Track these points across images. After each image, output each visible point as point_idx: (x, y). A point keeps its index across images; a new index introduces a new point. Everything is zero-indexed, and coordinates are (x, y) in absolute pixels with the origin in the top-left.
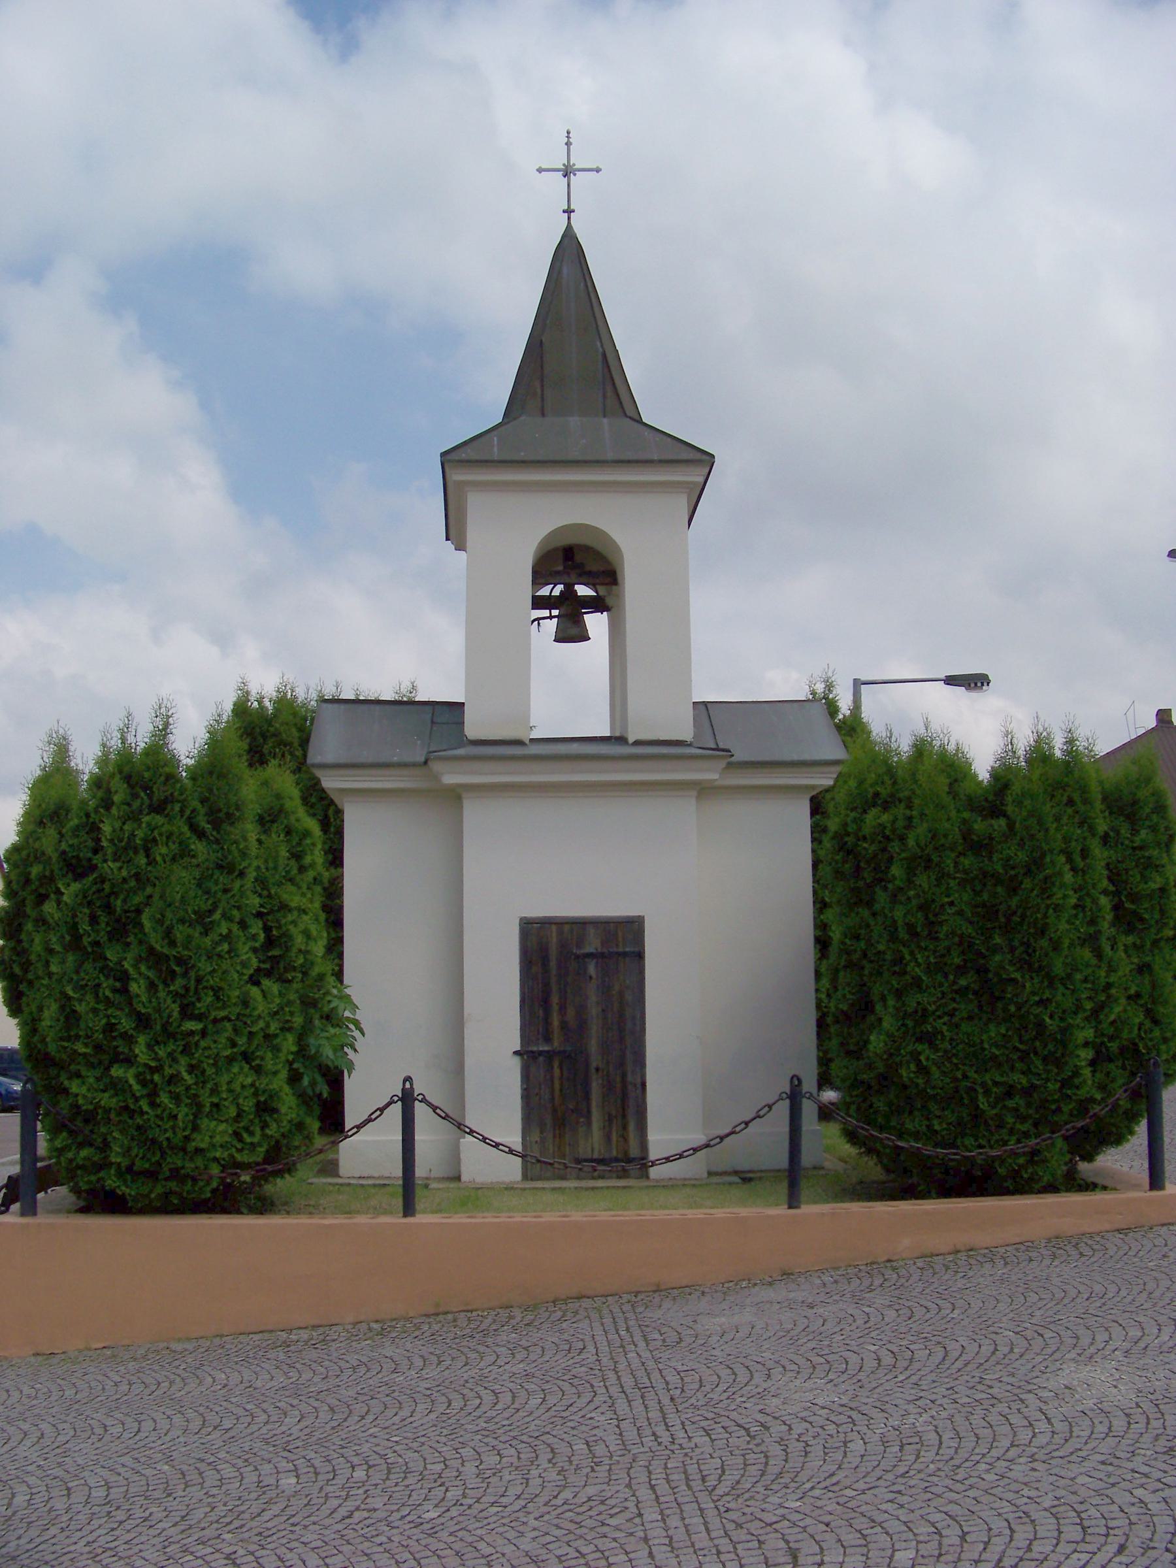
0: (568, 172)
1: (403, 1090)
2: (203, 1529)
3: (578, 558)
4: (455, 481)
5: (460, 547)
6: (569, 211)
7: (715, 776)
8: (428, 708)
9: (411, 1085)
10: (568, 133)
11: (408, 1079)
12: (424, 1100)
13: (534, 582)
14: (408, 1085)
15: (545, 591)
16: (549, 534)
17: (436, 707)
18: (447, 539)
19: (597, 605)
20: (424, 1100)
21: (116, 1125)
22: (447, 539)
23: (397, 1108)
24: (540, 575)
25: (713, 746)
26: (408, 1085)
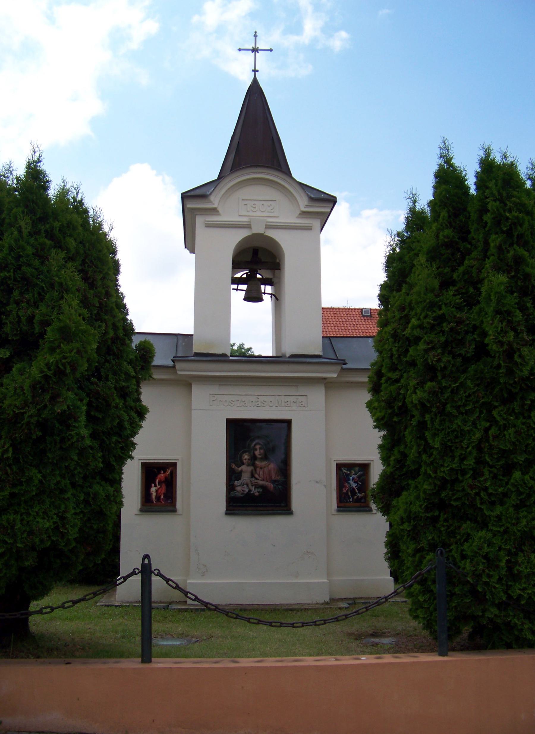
0: (255, 50)
1: (143, 565)
2: (90, 628)
3: (260, 255)
4: (188, 208)
5: (192, 251)
6: (255, 71)
7: (335, 375)
8: (174, 337)
9: (149, 561)
10: (256, 32)
11: (147, 556)
12: (160, 574)
13: (233, 268)
14: (146, 561)
15: (238, 275)
16: (242, 240)
17: (179, 336)
18: (186, 248)
19: (267, 282)
20: (160, 574)
21: (498, 258)
22: (186, 248)
23: (138, 578)
24: (236, 265)
25: (336, 358)
26: (146, 561)
